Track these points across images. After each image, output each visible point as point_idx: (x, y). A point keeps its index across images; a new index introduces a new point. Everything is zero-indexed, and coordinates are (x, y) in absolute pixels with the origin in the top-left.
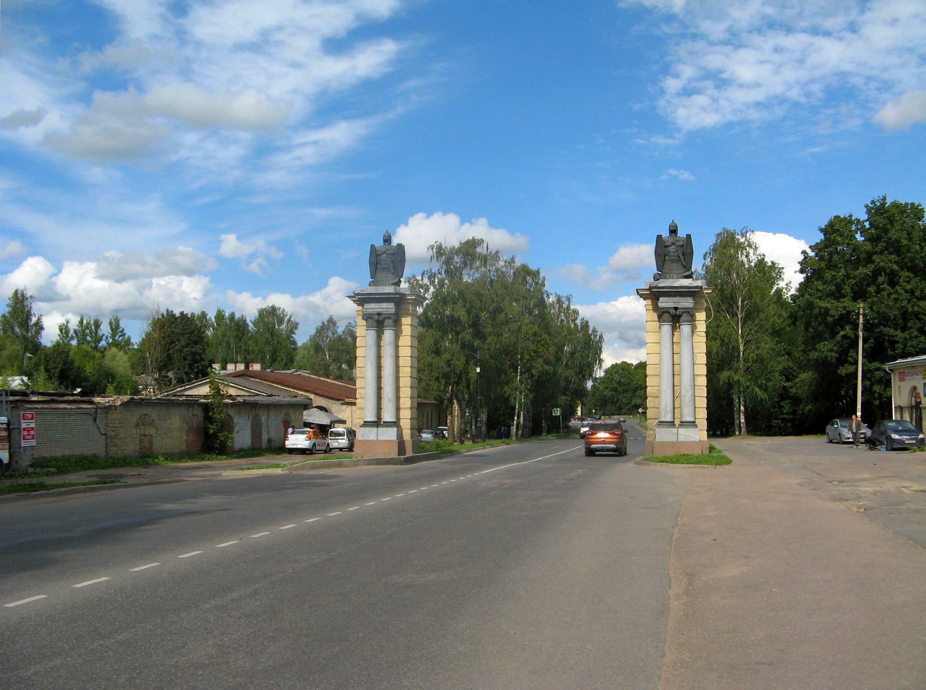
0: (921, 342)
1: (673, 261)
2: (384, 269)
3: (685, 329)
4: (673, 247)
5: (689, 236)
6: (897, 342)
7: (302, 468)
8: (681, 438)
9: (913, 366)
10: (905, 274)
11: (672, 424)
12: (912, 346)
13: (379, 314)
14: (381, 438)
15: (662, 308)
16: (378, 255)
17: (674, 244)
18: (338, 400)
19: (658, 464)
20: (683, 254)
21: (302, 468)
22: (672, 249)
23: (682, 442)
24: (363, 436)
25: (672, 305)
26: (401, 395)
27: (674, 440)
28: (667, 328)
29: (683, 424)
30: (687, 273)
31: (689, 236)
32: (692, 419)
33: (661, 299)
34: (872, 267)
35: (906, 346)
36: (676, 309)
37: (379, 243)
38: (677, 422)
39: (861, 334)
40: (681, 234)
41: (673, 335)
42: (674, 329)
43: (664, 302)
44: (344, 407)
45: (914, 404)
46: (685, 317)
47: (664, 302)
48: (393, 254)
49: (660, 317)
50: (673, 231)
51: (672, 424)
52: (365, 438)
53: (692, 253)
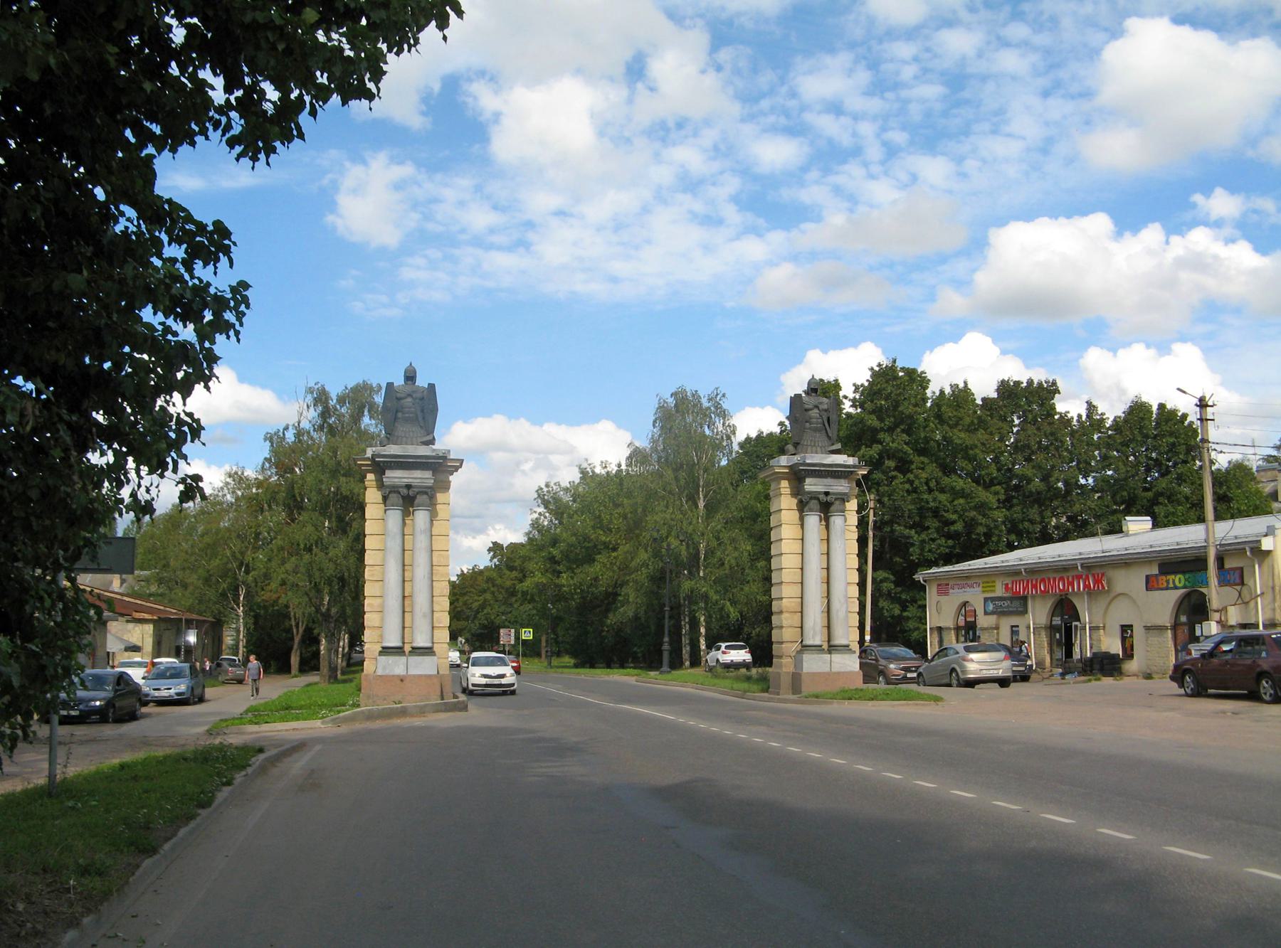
0: (940, 545)
1: (816, 430)
2: (407, 420)
3: (421, 517)
4: (409, 400)
5: (432, 386)
6: (913, 545)
7: (257, 715)
8: (836, 668)
9: (967, 577)
10: (917, 459)
11: (398, 651)
12: (930, 551)
13: (409, 487)
14: (413, 672)
15: (810, 493)
16: (399, 399)
17: (409, 395)
18: (123, 615)
19: (846, 702)
20: (422, 411)
21: (257, 715)
22: (815, 413)
23: (839, 673)
24: (384, 668)
25: (821, 489)
26: (436, 608)
27: (827, 670)
28: (813, 520)
29: (417, 651)
30: (425, 439)
31: (432, 386)
32: (429, 645)
33: (808, 481)
34: (877, 447)
35: (922, 549)
36: (827, 494)
37: (399, 381)
38: (407, 648)
39: (871, 533)
40: (422, 382)
41: (404, 524)
42: (826, 520)
43: (811, 485)
44: (131, 626)
45: (961, 623)
46: (420, 499)
47: (811, 485)
48: (422, 399)
49: (385, 499)
50: (410, 377)
51: (398, 651)
52: (387, 672)
53: (434, 410)
